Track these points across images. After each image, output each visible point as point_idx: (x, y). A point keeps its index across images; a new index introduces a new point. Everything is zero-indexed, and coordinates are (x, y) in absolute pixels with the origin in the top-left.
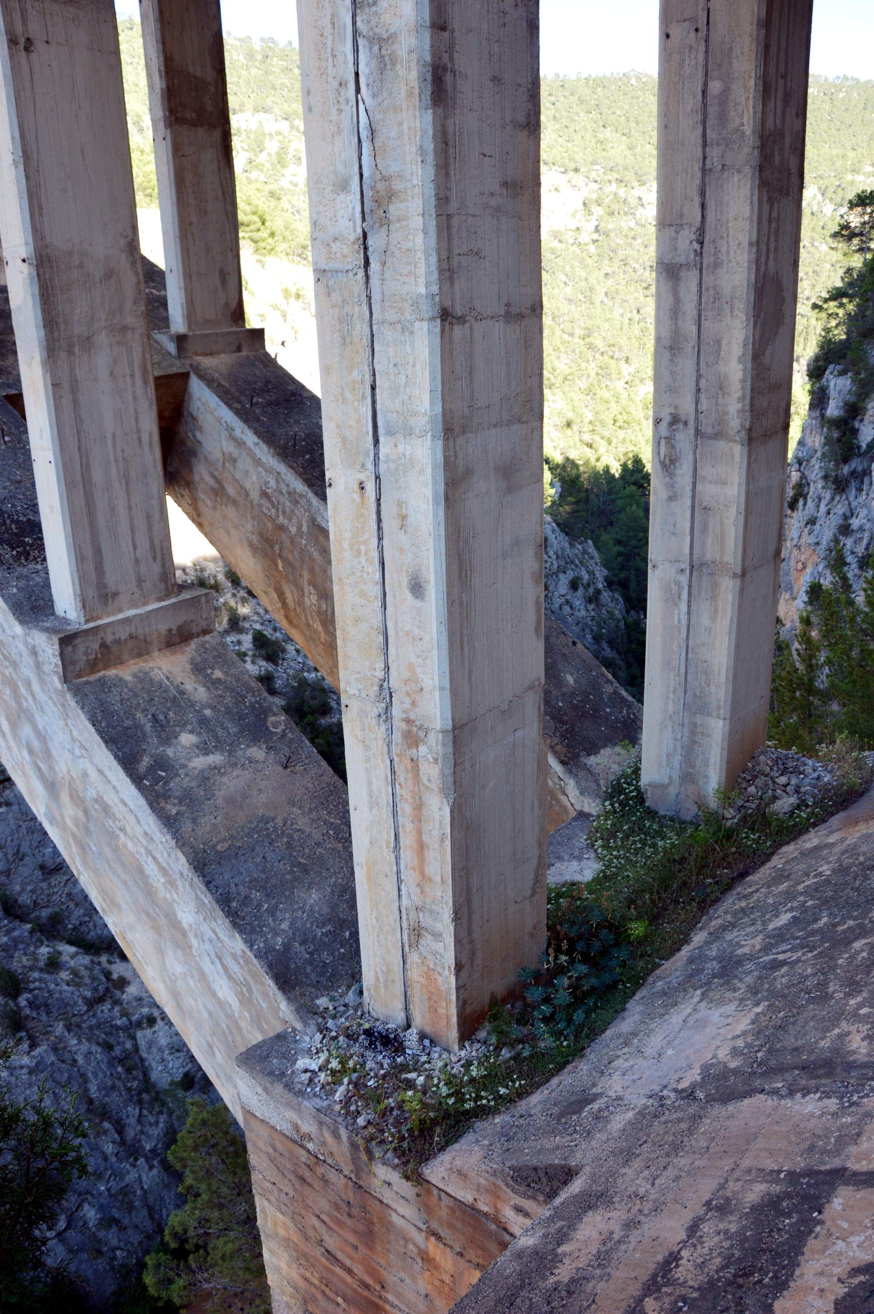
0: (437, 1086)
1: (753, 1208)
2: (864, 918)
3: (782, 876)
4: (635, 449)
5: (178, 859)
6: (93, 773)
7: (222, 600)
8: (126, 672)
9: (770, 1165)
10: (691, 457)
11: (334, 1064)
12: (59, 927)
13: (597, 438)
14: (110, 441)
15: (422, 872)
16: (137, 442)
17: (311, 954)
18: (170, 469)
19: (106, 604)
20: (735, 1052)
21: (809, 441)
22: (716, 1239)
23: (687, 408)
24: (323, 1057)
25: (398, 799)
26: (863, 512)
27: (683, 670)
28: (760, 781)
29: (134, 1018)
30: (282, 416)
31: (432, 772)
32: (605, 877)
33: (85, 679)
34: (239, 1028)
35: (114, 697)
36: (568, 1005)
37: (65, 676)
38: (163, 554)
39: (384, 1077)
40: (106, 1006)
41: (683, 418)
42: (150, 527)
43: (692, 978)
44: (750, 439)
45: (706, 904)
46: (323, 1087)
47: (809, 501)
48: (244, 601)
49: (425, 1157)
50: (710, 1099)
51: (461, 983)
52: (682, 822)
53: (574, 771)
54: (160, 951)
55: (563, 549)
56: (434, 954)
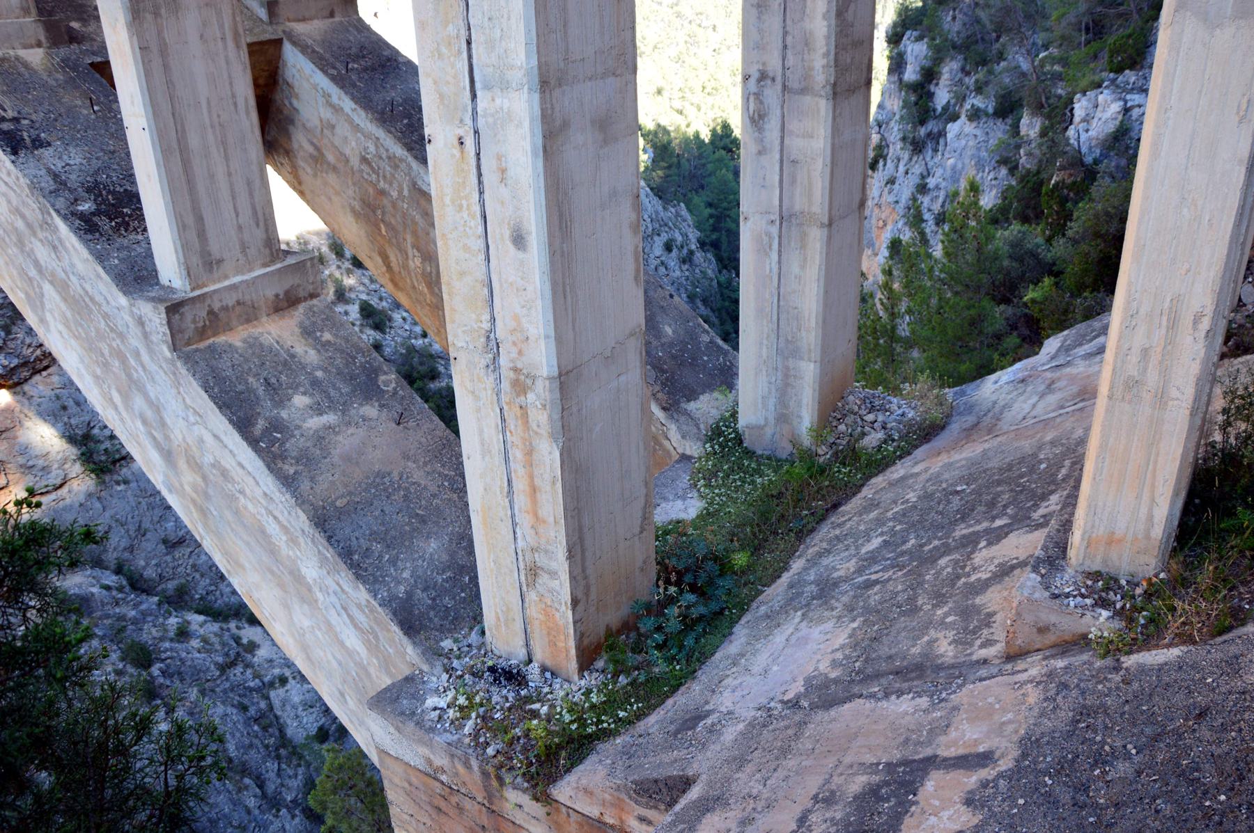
0: (560, 713)
1: (856, 798)
2: (948, 538)
3: (872, 505)
4: (724, 115)
5: (298, 517)
6: (208, 438)
7: (327, 272)
8: (236, 338)
9: (870, 759)
10: (778, 112)
11: (462, 700)
12: (187, 598)
13: (687, 104)
14: (204, 105)
15: (536, 515)
16: (232, 108)
17: (434, 599)
18: (269, 138)
19: (211, 271)
20: (835, 664)
21: (888, 104)
22: (824, 827)
23: (774, 65)
24: (451, 694)
25: (509, 446)
26: (939, 172)
27: (775, 318)
28: (849, 420)
29: (266, 679)
30: (379, 82)
31: (541, 418)
32: (708, 514)
33: (194, 347)
34: (368, 675)
35: (224, 364)
36: (680, 632)
37: (174, 344)
38: (266, 220)
39: (510, 709)
40: (239, 669)
41: (771, 75)
42: (251, 195)
43: (790, 604)
44: (835, 94)
45: (802, 534)
46: (452, 722)
47: (889, 161)
48: (349, 272)
49: (553, 779)
50: (814, 707)
51: (577, 617)
52: (778, 460)
53: (675, 416)
54: (287, 607)
55: (657, 212)
56: (551, 591)
